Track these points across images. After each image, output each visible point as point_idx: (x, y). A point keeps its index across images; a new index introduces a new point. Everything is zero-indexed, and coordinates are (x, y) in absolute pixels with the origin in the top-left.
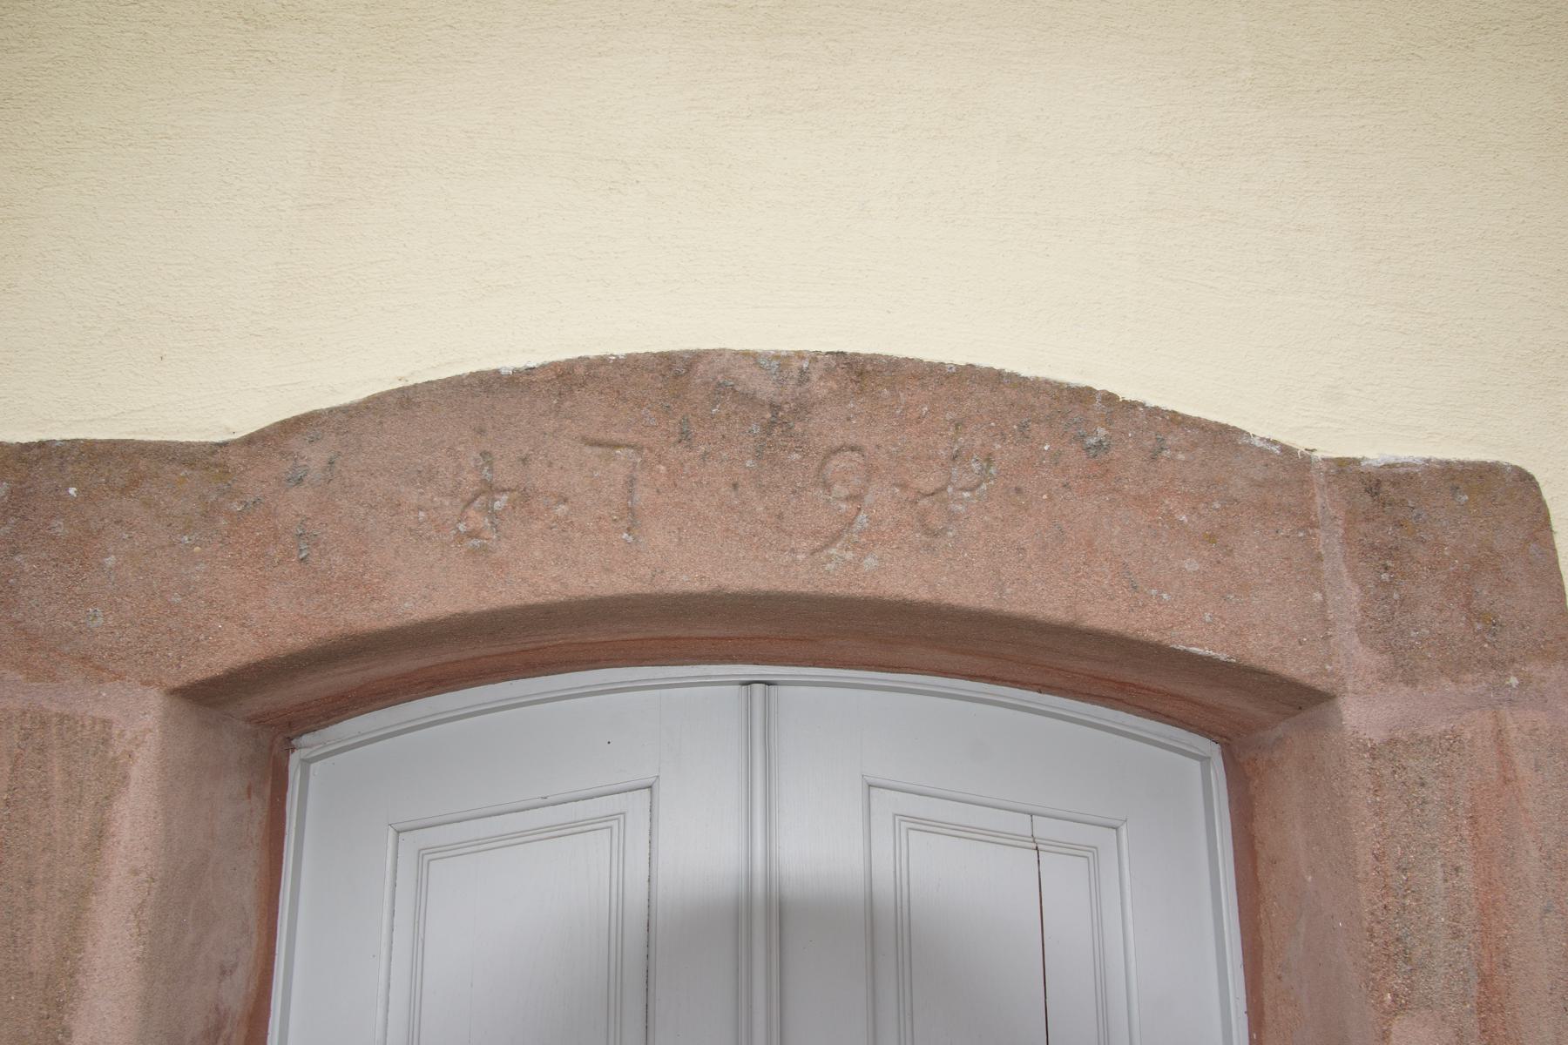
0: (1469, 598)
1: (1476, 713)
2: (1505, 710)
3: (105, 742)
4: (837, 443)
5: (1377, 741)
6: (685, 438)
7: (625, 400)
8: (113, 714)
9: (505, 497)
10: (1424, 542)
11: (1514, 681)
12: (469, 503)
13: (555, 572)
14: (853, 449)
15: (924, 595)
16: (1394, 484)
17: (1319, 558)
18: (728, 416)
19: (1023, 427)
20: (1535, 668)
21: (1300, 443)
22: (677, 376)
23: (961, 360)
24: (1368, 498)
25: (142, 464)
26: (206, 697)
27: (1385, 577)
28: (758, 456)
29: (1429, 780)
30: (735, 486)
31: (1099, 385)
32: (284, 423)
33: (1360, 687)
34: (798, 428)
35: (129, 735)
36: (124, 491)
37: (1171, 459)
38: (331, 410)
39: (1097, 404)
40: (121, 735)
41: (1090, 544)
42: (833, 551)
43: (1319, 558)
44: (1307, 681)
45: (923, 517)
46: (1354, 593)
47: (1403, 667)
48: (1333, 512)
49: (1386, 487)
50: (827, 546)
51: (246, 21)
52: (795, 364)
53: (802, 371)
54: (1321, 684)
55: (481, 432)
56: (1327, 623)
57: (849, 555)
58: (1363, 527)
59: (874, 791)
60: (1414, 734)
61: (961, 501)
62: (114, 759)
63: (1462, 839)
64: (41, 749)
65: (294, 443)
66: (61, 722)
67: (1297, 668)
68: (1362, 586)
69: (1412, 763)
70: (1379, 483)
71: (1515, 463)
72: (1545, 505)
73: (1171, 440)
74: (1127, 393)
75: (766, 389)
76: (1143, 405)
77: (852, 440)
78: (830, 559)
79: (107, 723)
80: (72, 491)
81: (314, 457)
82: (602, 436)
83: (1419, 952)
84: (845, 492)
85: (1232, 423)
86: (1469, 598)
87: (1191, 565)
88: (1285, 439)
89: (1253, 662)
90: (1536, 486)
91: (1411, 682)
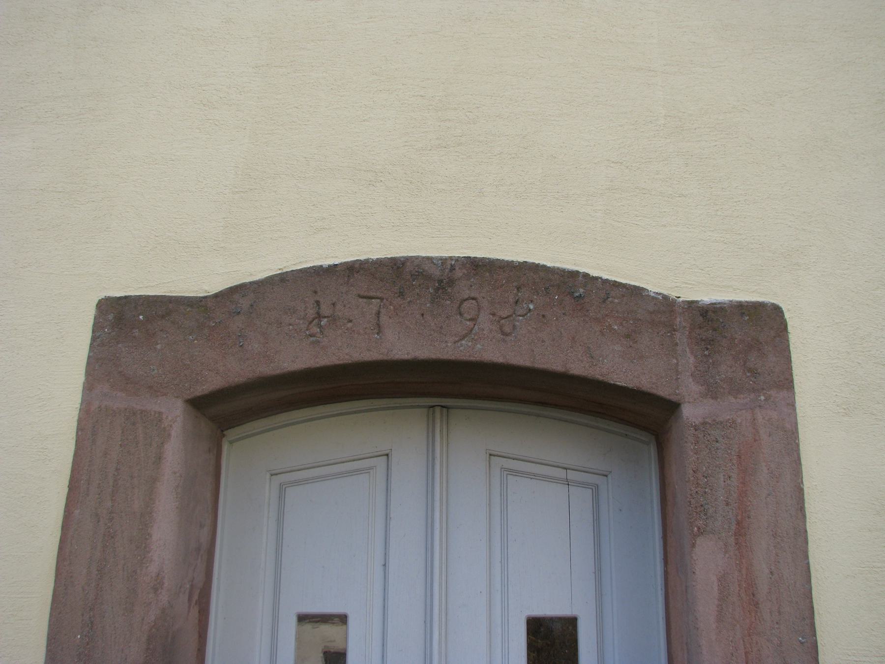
0: (745, 362)
1: (744, 411)
2: (757, 410)
3: (160, 421)
4: (466, 297)
5: (697, 423)
6: (401, 294)
7: (376, 278)
8: (163, 410)
9: (326, 320)
10: (726, 337)
11: (762, 398)
12: (311, 323)
13: (347, 351)
14: (473, 299)
15: (501, 360)
16: (714, 312)
17: (677, 344)
18: (420, 285)
19: (546, 289)
20: (773, 392)
21: (673, 294)
22: (398, 268)
23: (521, 260)
24: (701, 318)
25: (171, 306)
26: (199, 404)
27: (706, 353)
28: (432, 302)
29: (720, 439)
30: (423, 315)
31: (582, 270)
32: (231, 288)
33: (691, 400)
34: (449, 290)
35: (170, 418)
36: (163, 317)
37: (612, 302)
38: (250, 283)
39: (580, 278)
40: (167, 418)
41: (573, 338)
42: (463, 342)
43: (677, 344)
44: (668, 397)
45: (501, 328)
46: (692, 360)
47: (712, 392)
48: (684, 324)
49: (710, 313)
50: (461, 340)
51: (204, 105)
52: (449, 262)
53: (451, 265)
54: (674, 398)
55: (316, 292)
56: (678, 373)
57: (470, 344)
58: (698, 331)
59: (492, 457)
60: (714, 420)
61: (518, 321)
62: (164, 428)
63: (733, 464)
64: (134, 424)
65: (236, 296)
66: (141, 413)
67: (663, 392)
68: (696, 356)
69: (713, 432)
70: (707, 312)
71: (773, 301)
72: (785, 320)
73: (613, 293)
74: (594, 273)
75: (437, 273)
76: (601, 278)
77: (473, 295)
78: (462, 345)
79: (160, 413)
80: (141, 317)
81: (244, 303)
82: (366, 294)
83: (711, 511)
84: (469, 317)
85: (642, 285)
86: (745, 362)
87: (618, 348)
88: (665, 292)
89: (644, 389)
90: (782, 312)
91: (715, 398)
